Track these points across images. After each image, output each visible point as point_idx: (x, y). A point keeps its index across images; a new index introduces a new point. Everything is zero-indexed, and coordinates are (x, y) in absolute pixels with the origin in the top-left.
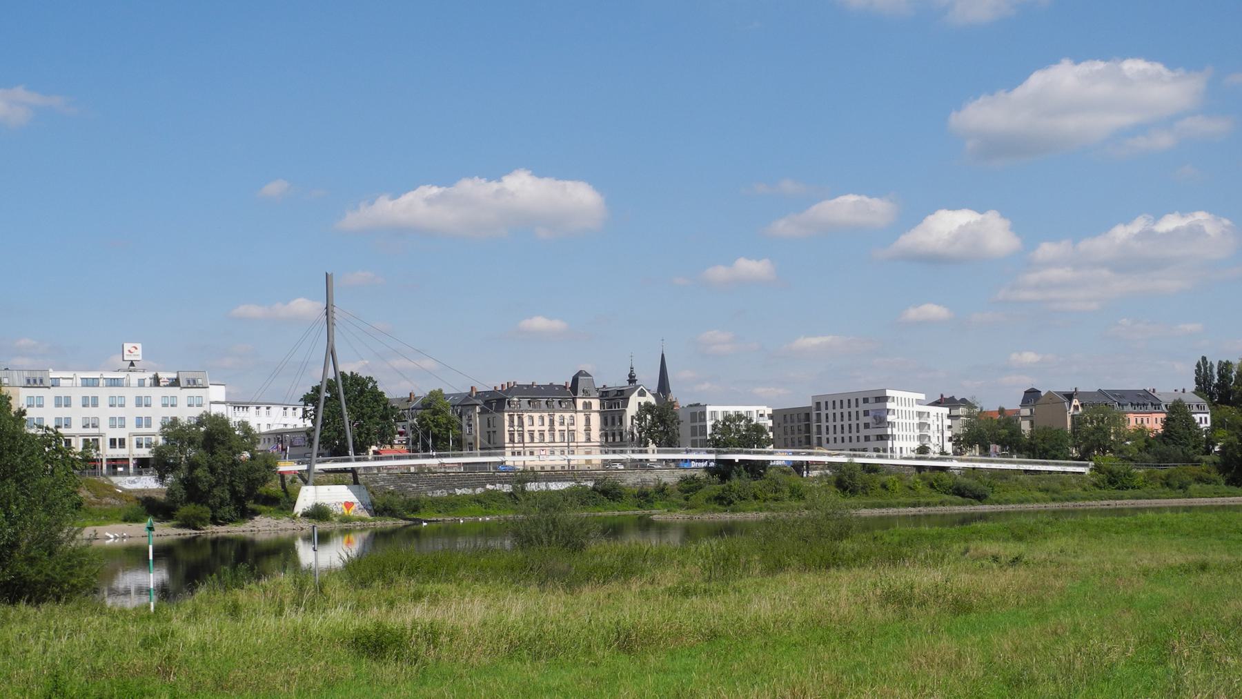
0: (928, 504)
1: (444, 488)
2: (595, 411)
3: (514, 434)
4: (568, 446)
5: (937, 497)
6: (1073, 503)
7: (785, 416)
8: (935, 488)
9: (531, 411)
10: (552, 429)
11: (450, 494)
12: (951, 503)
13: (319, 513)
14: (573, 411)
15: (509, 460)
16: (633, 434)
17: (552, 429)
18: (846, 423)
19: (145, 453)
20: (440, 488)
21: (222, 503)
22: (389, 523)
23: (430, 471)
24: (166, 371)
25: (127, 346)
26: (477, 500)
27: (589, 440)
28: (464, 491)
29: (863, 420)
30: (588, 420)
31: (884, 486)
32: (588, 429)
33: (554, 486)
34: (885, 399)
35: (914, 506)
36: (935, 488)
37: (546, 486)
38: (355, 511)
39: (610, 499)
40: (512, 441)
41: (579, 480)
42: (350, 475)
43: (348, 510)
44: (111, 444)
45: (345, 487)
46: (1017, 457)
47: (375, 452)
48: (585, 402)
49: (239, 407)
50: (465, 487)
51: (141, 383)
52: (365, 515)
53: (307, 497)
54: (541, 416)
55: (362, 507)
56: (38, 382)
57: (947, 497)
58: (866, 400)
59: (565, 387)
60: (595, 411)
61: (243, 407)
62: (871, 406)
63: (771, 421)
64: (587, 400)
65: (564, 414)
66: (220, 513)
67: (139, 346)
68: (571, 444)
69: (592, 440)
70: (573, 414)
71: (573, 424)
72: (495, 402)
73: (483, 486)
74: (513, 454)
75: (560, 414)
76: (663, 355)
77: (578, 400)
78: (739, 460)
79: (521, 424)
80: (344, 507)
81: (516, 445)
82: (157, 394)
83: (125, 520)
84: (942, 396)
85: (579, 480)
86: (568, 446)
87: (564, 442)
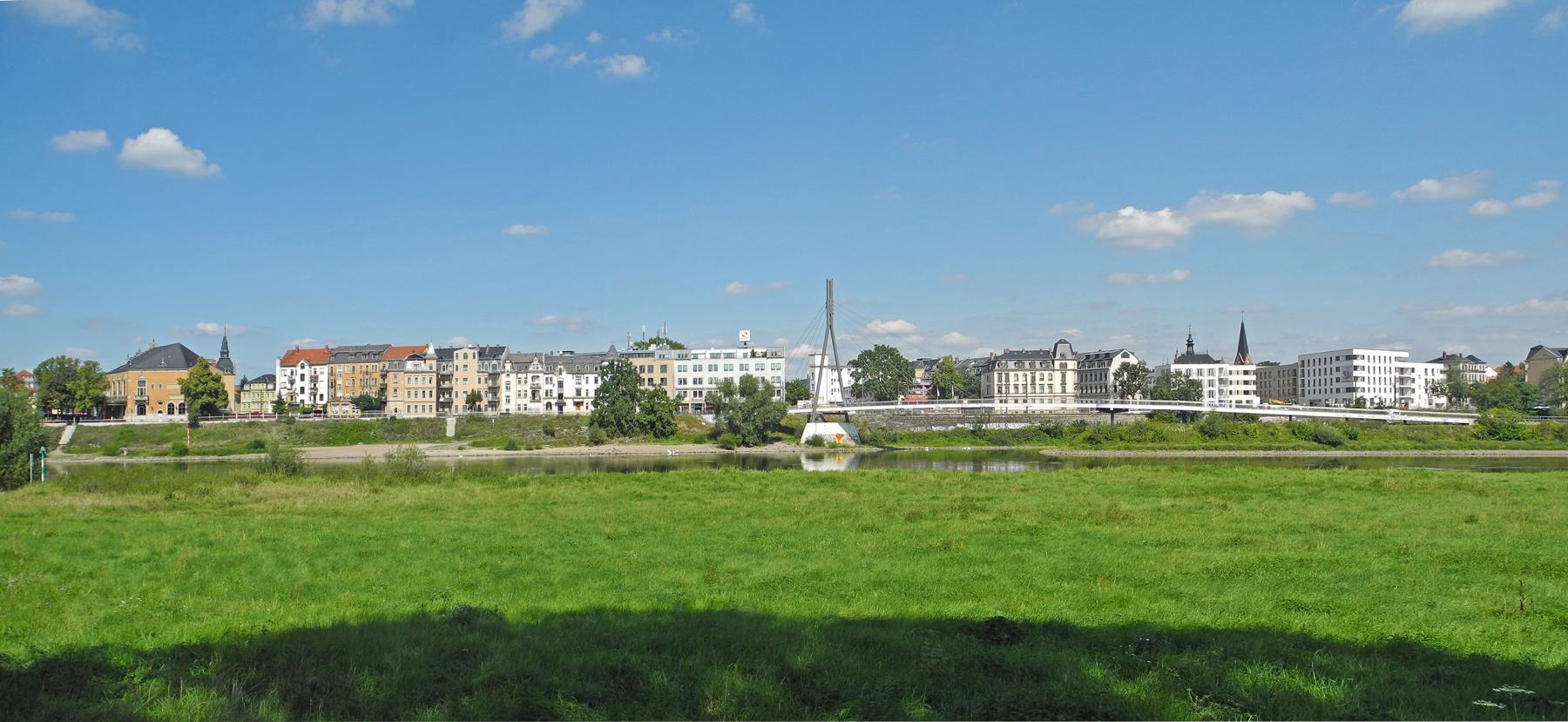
0: (1279, 449)
5: (1295, 442)
9: (1016, 370)
10: (1033, 383)
12: (1304, 448)
13: (816, 441)
15: (997, 406)
16: (1115, 387)
17: (1033, 383)
22: (866, 449)
24: (758, 347)
25: (742, 333)
26: (944, 435)
28: (938, 428)
29: (1336, 375)
30: (1064, 376)
31: (1246, 432)
32: (1063, 383)
33: (1011, 426)
34: (1351, 357)
35: (1265, 449)
40: (1000, 392)
42: (844, 416)
45: (837, 424)
47: (903, 400)
51: (745, 356)
52: (852, 443)
53: (811, 430)
57: (1302, 443)
58: (1337, 359)
62: (1343, 363)
63: (799, 402)
64: (1063, 362)
65: (1044, 372)
66: (747, 440)
71: (1051, 380)
72: (990, 365)
73: (955, 424)
74: (1001, 402)
76: (1242, 324)
82: (752, 362)
83: (695, 442)
84: (1444, 353)
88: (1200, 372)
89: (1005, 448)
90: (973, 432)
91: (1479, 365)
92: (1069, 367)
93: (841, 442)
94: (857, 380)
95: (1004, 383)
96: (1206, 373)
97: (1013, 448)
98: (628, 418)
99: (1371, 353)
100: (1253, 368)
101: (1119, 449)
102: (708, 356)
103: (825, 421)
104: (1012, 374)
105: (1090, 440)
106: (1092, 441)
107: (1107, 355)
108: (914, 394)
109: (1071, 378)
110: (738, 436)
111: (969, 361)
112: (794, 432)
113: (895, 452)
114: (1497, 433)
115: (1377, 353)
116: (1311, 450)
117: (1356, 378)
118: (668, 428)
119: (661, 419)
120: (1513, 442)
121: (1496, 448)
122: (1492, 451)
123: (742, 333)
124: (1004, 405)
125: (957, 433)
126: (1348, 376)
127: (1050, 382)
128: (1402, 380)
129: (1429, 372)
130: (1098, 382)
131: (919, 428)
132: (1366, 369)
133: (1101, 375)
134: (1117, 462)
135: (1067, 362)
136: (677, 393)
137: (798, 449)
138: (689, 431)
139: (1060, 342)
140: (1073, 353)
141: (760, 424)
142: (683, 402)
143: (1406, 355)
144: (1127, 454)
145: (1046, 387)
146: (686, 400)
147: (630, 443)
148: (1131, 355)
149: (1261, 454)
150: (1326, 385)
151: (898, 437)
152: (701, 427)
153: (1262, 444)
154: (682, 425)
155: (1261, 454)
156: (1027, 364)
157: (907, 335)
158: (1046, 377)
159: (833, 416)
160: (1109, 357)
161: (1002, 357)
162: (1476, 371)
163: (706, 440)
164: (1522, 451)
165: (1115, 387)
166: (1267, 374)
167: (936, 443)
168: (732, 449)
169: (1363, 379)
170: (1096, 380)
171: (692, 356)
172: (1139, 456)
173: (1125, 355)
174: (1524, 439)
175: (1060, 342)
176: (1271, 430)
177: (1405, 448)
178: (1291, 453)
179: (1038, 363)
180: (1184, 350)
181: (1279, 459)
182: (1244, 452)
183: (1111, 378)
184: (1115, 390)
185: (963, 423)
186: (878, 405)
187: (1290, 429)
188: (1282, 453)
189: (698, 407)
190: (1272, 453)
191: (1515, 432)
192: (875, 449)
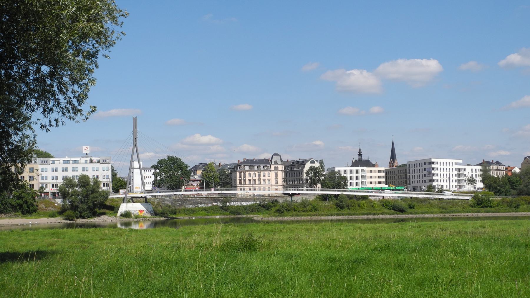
0: (374, 214)
1: (193, 204)
2: (280, 171)
3: (241, 181)
4: (253, 186)
6: (451, 214)
7: (399, 171)
8: (384, 206)
9: (249, 171)
10: (259, 179)
11: (196, 207)
12: (387, 214)
13: (127, 215)
14: (269, 171)
15: (239, 192)
16: (307, 180)
17: (259, 179)
18: (445, 173)
19: (55, 190)
20: (191, 204)
21: (84, 210)
22: (157, 219)
23: (188, 197)
24: (95, 157)
26: (205, 209)
27: (277, 183)
28: (202, 205)
30: (276, 175)
32: (276, 178)
33: (244, 204)
35: (367, 214)
36: (384, 206)
37: (241, 203)
38: (144, 214)
39: (266, 209)
40: (240, 183)
41: (256, 201)
43: (141, 213)
44: (103, 185)
46: (215, 190)
48: (275, 167)
49: (147, 170)
50: (203, 204)
51: (86, 162)
52: (149, 215)
53: (124, 208)
54: (264, 173)
55: (147, 212)
56: (46, 162)
59: (268, 160)
60: (280, 171)
61: (149, 170)
63: (120, 190)
64: (276, 166)
65: (265, 172)
66: (83, 214)
67: (88, 147)
68: (254, 185)
69: (278, 183)
70: (270, 172)
72: (235, 168)
73: (212, 203)
75: (263, 172)
76: (393, 142)
77: (272, 166)
78: (292, 193)
79: (245, 177)
80: (139, 212)
81: (242, 186)
82: (90, 166)
83: (49, 217)
84: (483, 160)
85: (256, 201)
86: (253, 186)
87: (251, 184)
88: (345, 172)
89: (239, 216)
90: (222, 208)
91: (501, 167)
92: (279, 169)
93: (142, 214)
94: (156, 177)
95: (242, 178)
96: (348, 172)
97: (244, 216)
98: (3, 202)
99: (442, 160)
100: (383, 169)
101: (293, 216)
102: (62, 162)
103: (134, 202)
104: (247, 173)
105: (279, 211)
106: (280, 212)
107: (303, 162)
108: (192, 185)
109: (281, 175)
110: (77, 212)
111: (226, 165)
112: (113, 209)
113: (175, 220)
114: (480, 204)
115: (445, 161)
116: (390, 214)
117: (434, 175)
118: (31, 208)
119: (26, 202)
120: (488, 209)
121: (479, 212)
122: (477, 214)
123: (84, 147)
124: (242, 192)
125: (213, 208)
126: (430, 174)
127: (269, 178)
128: (459, 175)
129: (474, 170)
130: (298, 177)
131: (191, 206)
132: (439, 169)
133: (299, 173)
134: (293, 222)
135: (278, 166)
136: (40, 185)
137: (115, 220)
138: (46, 210)
139: (275, 155)
140: (282, 161)
141: (91, 204)
142: (45, 191)
143: (461, 161)
144: (296, 218)
145: (267, 181)
146: (47, 190)
147: (4, 218)
148: (316, 162)
149: (365, 217)
150: (417, 179)
151: (177, 211)
152: (55, 207)
153: (366, 212)
154: (42, 206)
155: (365, 217)
156: (256, 167)
157: (212, 145)
158: (267, 175)
159: (139, 199)
160: (303, 163)
161: (242, 163)
162: (500, 170)
163: (57, 215)
164: (491, 214)
165: (307, 180)
166: (393, 172)
167: (200, 214)
168: (74, 220)
169: (437, 175)
170: (297, 176)
171: (51, 162)
172: (411, 217)
173: (313, 162)
174: (493, 207)
175: (275, 155)
176: (372, 204)
177: (436, 213)
178: (380, 217)
179: (262, 167)
180: (357, 158)
181: (375, 219)
182: (356, 216)
183: (305, 175)
184: (307, 182)
185: (216, 202)
186: (169, 192)
187: (382, 204)
188: (375, 217)
189: (54, 194)
190: (371, 217)
191: (489, 203)
192: (163, 219)
